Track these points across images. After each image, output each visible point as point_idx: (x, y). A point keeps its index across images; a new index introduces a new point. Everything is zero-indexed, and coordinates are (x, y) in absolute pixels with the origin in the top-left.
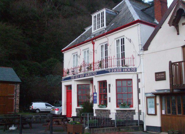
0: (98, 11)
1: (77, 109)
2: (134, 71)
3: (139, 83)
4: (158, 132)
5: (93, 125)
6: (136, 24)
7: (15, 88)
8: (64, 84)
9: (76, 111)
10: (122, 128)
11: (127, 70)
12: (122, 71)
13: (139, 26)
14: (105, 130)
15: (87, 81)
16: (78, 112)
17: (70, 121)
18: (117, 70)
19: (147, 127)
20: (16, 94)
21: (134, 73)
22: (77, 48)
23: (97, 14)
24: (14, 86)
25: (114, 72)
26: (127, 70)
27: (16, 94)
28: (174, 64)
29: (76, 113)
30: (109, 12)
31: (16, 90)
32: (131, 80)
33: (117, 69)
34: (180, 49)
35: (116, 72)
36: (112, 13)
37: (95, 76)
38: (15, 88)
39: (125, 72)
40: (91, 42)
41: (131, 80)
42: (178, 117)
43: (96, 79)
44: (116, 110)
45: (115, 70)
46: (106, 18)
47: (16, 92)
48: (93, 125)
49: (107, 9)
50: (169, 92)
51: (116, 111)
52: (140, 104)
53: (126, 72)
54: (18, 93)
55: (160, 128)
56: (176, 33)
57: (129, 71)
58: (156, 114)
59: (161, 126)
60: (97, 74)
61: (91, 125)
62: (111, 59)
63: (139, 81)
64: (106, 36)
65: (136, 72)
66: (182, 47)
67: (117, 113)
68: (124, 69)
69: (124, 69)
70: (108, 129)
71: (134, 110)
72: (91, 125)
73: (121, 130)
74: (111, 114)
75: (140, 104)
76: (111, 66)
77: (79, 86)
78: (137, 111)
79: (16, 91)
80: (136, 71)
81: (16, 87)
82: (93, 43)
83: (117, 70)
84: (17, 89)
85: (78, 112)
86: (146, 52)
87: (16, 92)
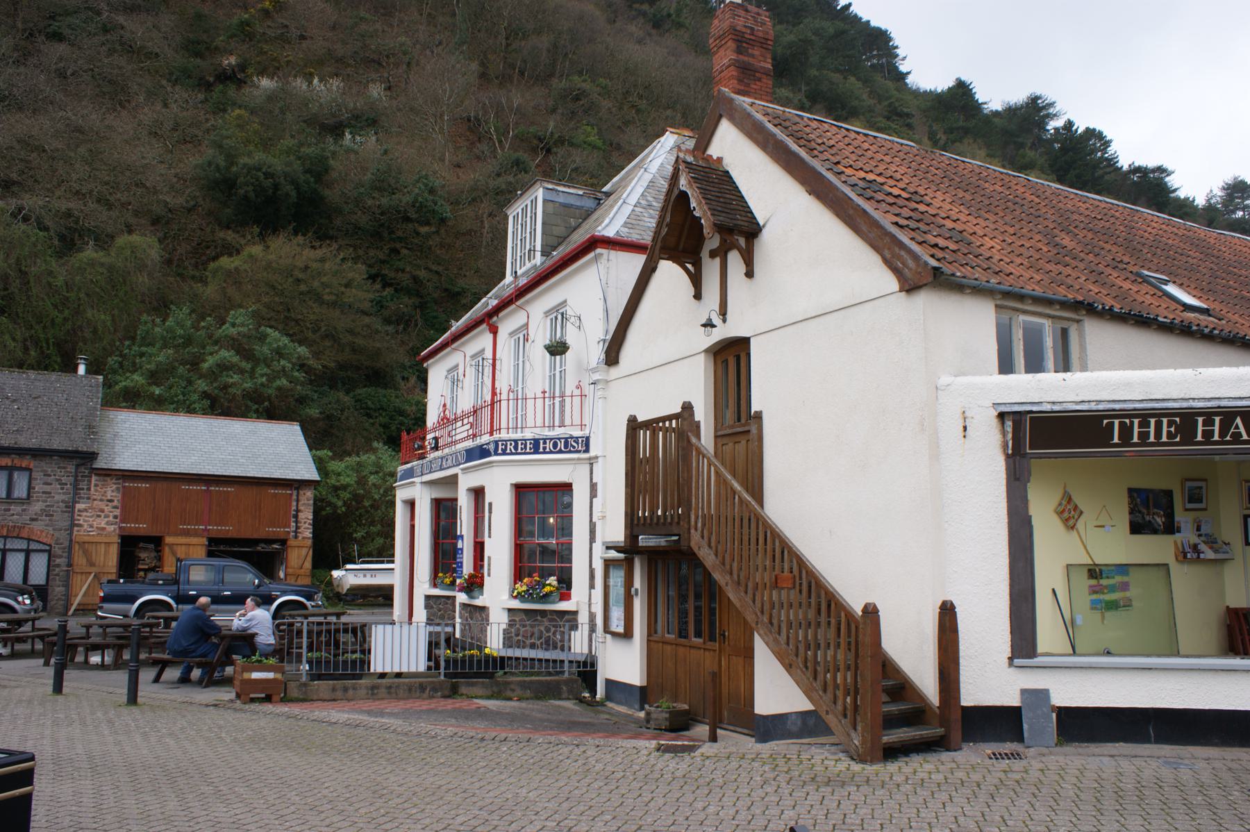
0: (521, 195)
1: (428, 597)
2: (578, 452)
3: (594, 500)
4: (630, 706)
5: (463, 667)
6: (592, 255)
7: (294, 504)
8: (401, 495)
9: (426, 607)
10: (469, 684)
11: (555, 445)
12: (536, 452)
13: (603, 260)
14: (383, 690)
15: (447, 483)
16: (432, 607)
17: (168, 643)
18: (516, 448)
19: (609, 683)
20: (297, 528)
21: (579, 459)
22: (456, 349)
23: (521, 207)
24: (291, 495)
25: (504, 453)
26: (555, 445)
27: (297, 528)
28: (650, 425)
29: (425, 612)
30: (561, 199)
31: (298, 511)
32: (567, 487)
33: (516, 441)
34: (702, 357)
35: (512, 454)
36: (572, 201)
37: (462, 466)
38: (294, 504)
39: (544, 452)
40: (484, 326)
41: (567, 487)
42: (693, 651)
43: (467, 482)
44: (510, 610)
45: (510, 448)
46: (544, 224)
47: (297, 522)
48: (463, 667)
49: (550, 186)
50: (623, 545)
51: (506, 612)
52: (594, 588)
53: (551, 452)
54: (307, 525)
55: (642, 689)
56: (692, 291)
57: (560, 452)
58: (627, 634)
59: (645, 684)
60: (468, 460)
61: (455, 667)
62: (500, 401)
63: (593, 488)
64: (518, 303)
65: (586, 456)
66: (707, 351)
67: (511, 624)
68: (545, 443)
69: (545, 443)
70: (398, 687)
71: (575, 613)
72: (455, 667)
73: (463, 690)
74: (580, 626)
75: (594, 588)
76: (500, 429)
77: (531, 497)
78: (583, 618)
79: (296, 516)
80: (587, 451)
81: (298, 501)
82: (494, 331)
83: (516, 448)
84: (301, 508)
85: (432, 607)
86: (615, 372)
87: (297, 522)
